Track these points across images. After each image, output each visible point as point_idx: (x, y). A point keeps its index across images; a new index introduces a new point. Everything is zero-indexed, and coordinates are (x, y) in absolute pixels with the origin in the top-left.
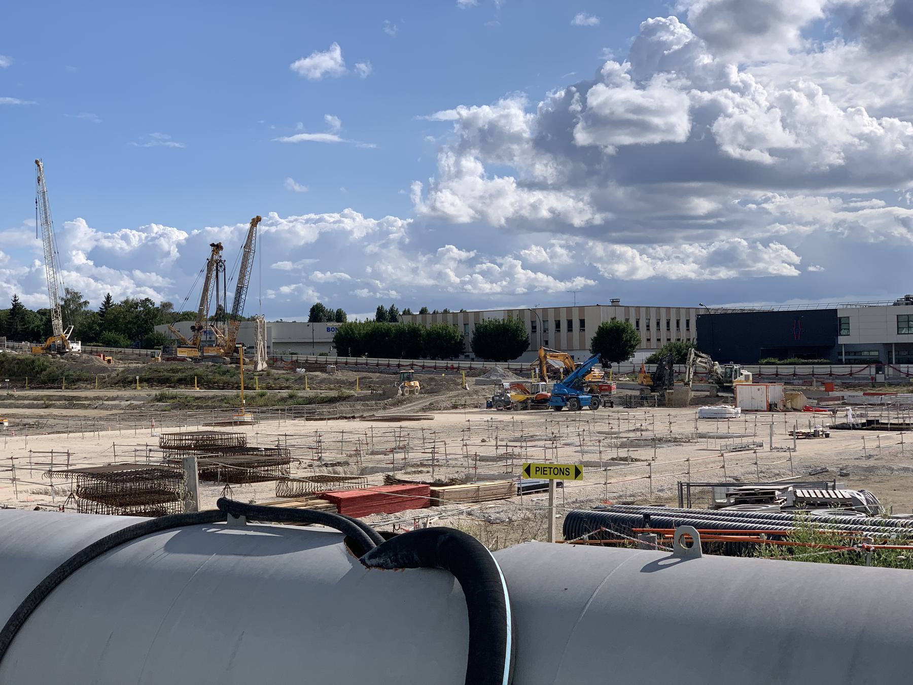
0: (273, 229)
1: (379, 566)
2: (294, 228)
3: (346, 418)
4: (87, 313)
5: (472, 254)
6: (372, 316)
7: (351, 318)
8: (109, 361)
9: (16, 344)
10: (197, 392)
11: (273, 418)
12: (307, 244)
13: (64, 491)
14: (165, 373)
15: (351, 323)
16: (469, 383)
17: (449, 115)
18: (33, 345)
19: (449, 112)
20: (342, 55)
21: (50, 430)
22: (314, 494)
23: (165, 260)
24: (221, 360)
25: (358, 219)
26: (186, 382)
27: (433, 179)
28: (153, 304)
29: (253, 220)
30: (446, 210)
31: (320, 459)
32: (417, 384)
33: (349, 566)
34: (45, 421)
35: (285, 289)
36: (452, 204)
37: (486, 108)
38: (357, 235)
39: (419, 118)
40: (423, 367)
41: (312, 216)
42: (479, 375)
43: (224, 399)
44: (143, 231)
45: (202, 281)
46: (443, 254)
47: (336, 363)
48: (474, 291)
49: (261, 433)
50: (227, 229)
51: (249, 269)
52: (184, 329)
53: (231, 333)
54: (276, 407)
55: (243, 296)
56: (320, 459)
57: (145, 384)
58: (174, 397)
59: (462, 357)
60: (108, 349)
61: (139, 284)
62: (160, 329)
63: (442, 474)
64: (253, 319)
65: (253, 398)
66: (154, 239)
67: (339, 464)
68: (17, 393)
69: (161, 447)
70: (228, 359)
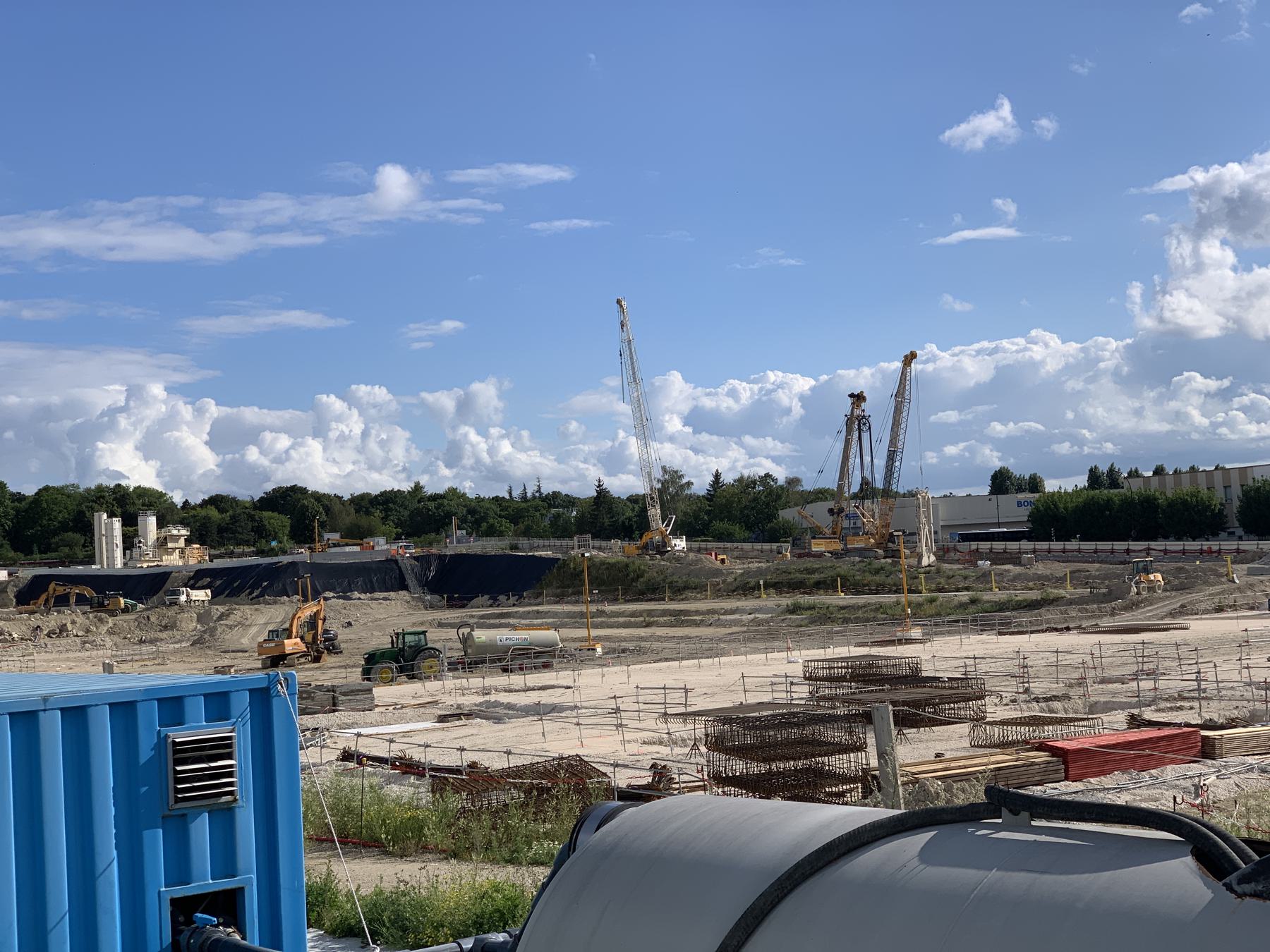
0: (930, 367)
1: (1255, 895)
2: (957, 363)
3: (1056, 630)
4: (690, 496)
5: (1226, 383)
6: (1082, 481)
7: (1051, 486)
8: (723, 561)
9: (604, 543)
10: (841, 598)
11: (950, 633)
12: (978, 385)
13: (683, 740)
14: (798, 575)
15: (1053, 494)
16: (1239, 574)
17: (1180, 182)
18: (626, 544)
19: (1179, 177)
20: (1013, 112)
21: (655, 657)
22: (1028, 743)
23: (785, 420)
24: (871, 554)
25: (1052, 344)
26: (827, 585)
27: (1159, 274)
28: (775, 480)
29: (906, 357)
30: (1179, 321)
31: (1027, 691)
32: (1159, 577)
33: (1208, 895)
34: (647, 644)
35: (951, 450)
36: (1190, 311)
37: (1234, 167)
38: (1052, 366)
39: (1133, 191)
40: (1165, 552)
41: (985, 344)
42: (1253, 561)
43: (879, 607)
44: (754, 382)
45: (840, 446)
46: (1180, 386)
47: (1034, 551)
48: (1233, 437)
49: (941, 654)
50: (867, 371)
51: (903, 426)
52: (818, 513)
53: (883, 515)
54: (953, 617)
55: (897, 464)
56: (1027, 691)
57: (772, 591)
58: (811, 608)
59: (1223, 535)
60: (721, 545)
61: (752, 454)
62: (787, 515)
63: (1213, 712)
64: (912, 494)
65: (919, 605)
66: (769, 392)
67: (1055, 698)
68: (609, 608)
69: (806, 679)
70: (880, 552)
